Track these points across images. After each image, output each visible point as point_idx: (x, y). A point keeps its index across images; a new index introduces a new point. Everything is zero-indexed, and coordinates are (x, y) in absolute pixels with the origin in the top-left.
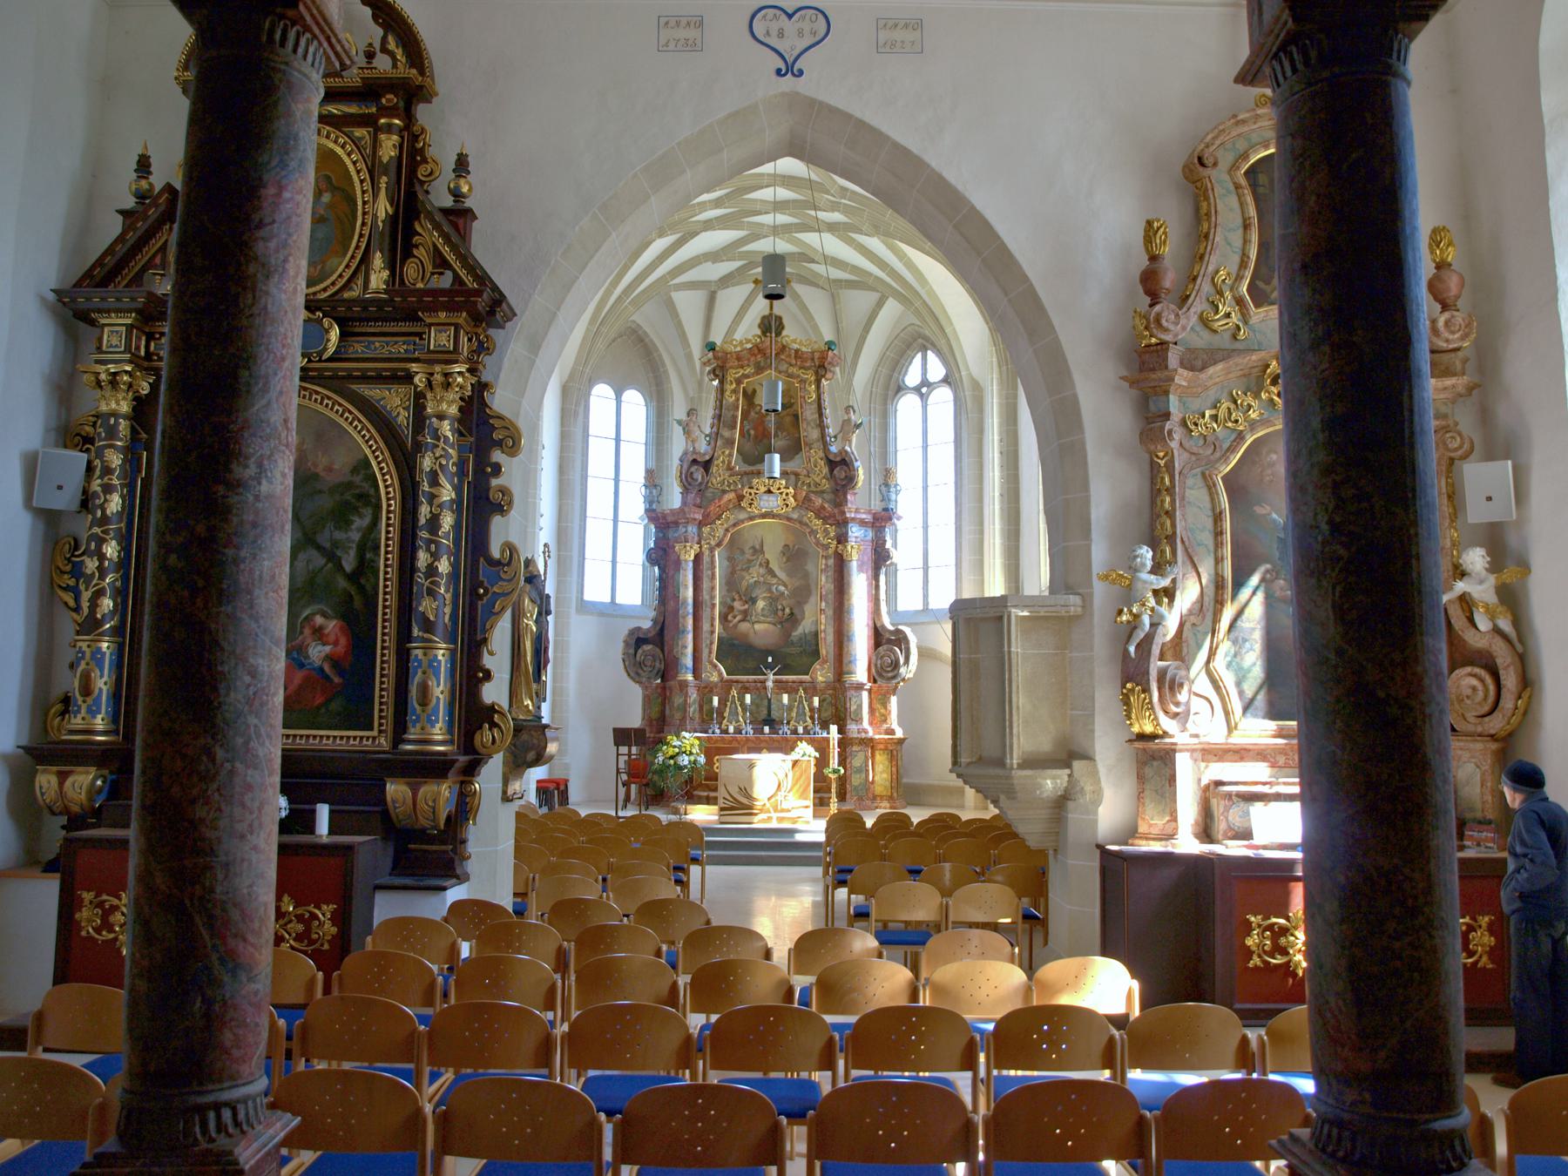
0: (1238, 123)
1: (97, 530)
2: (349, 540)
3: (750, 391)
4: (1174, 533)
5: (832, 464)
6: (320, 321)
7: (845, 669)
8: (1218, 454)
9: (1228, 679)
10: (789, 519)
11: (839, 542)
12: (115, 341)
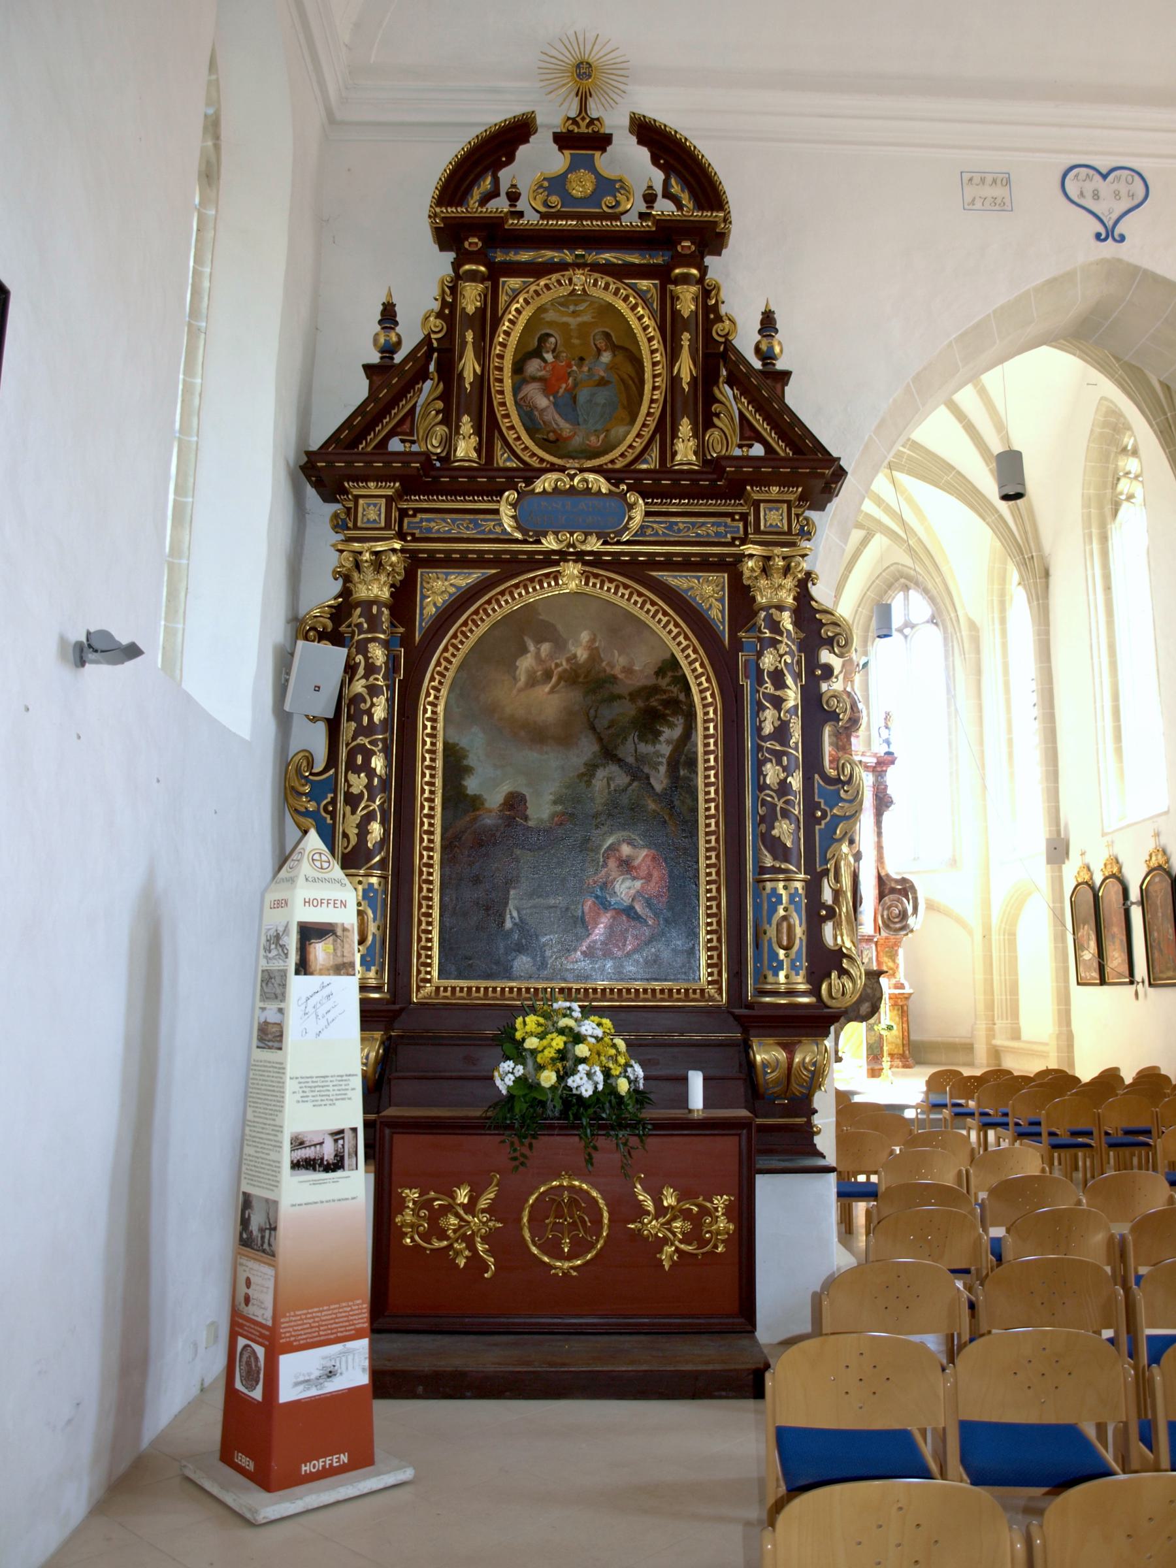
1: (362, 740)
2: (658, 754)
6: (623, 495)
12: (372, 516)
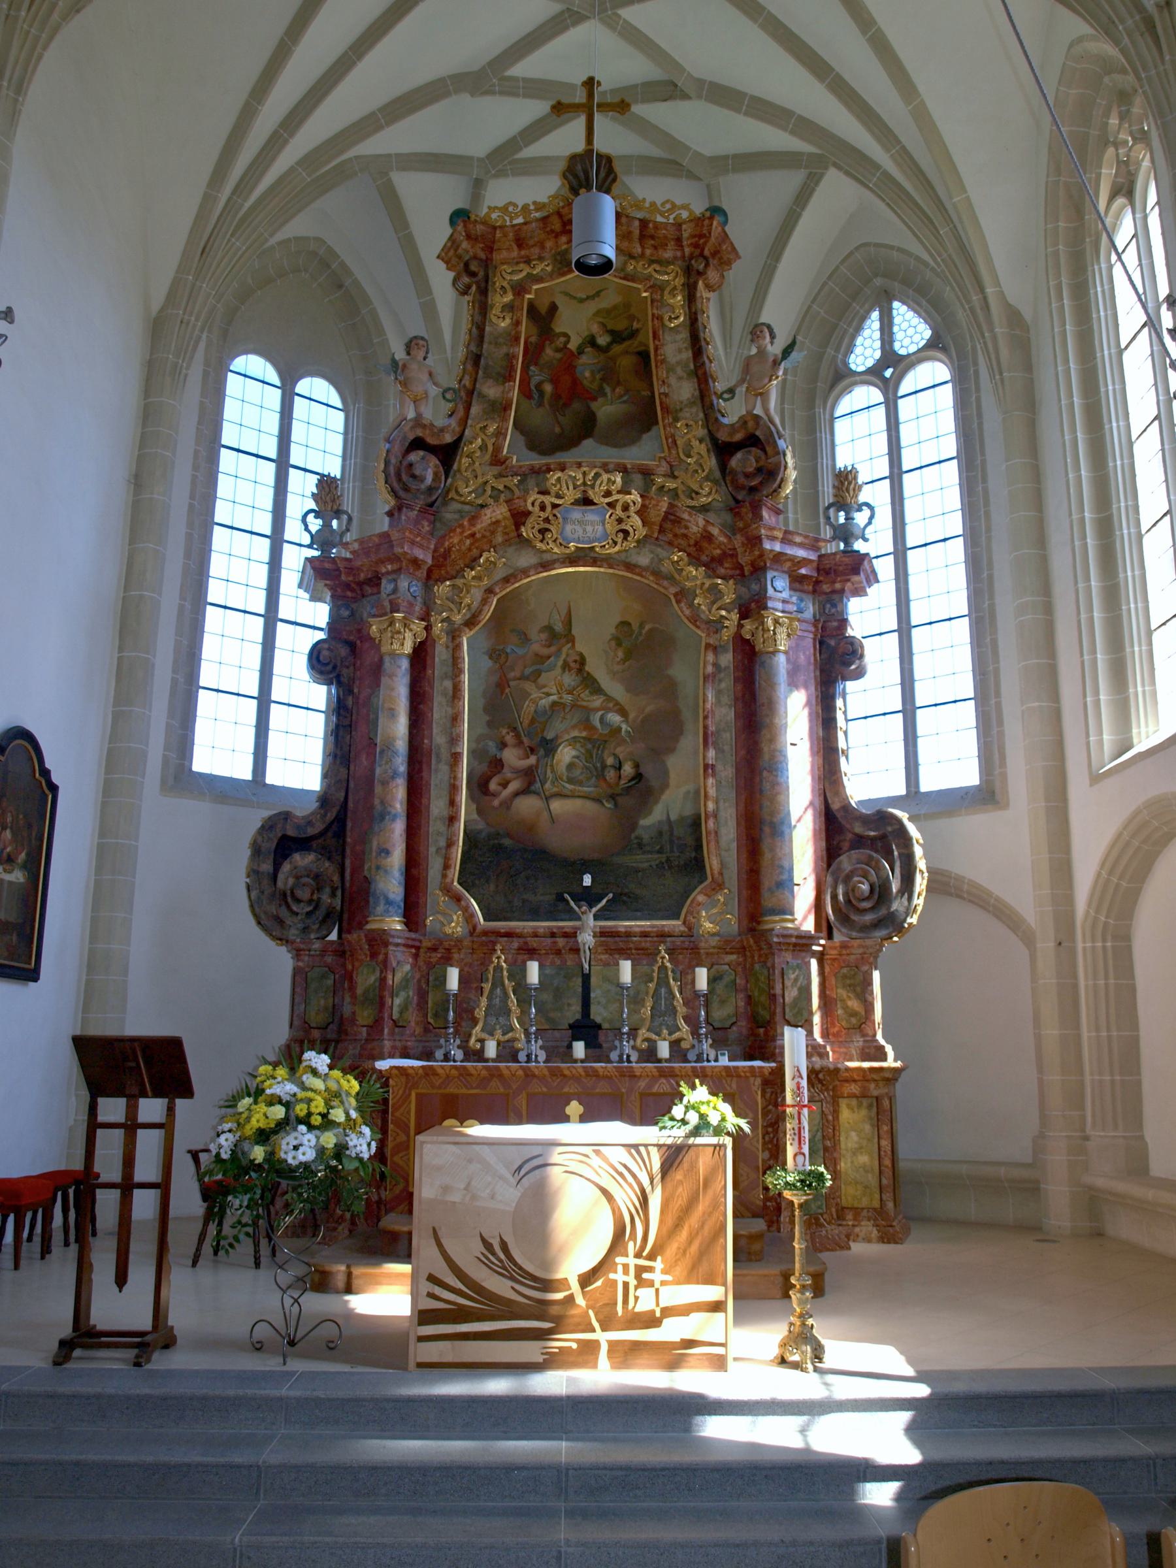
3: (543, 309)
5: (723, 450)
7: (768, 901)
10: (630, 567)
11: (744, 614)
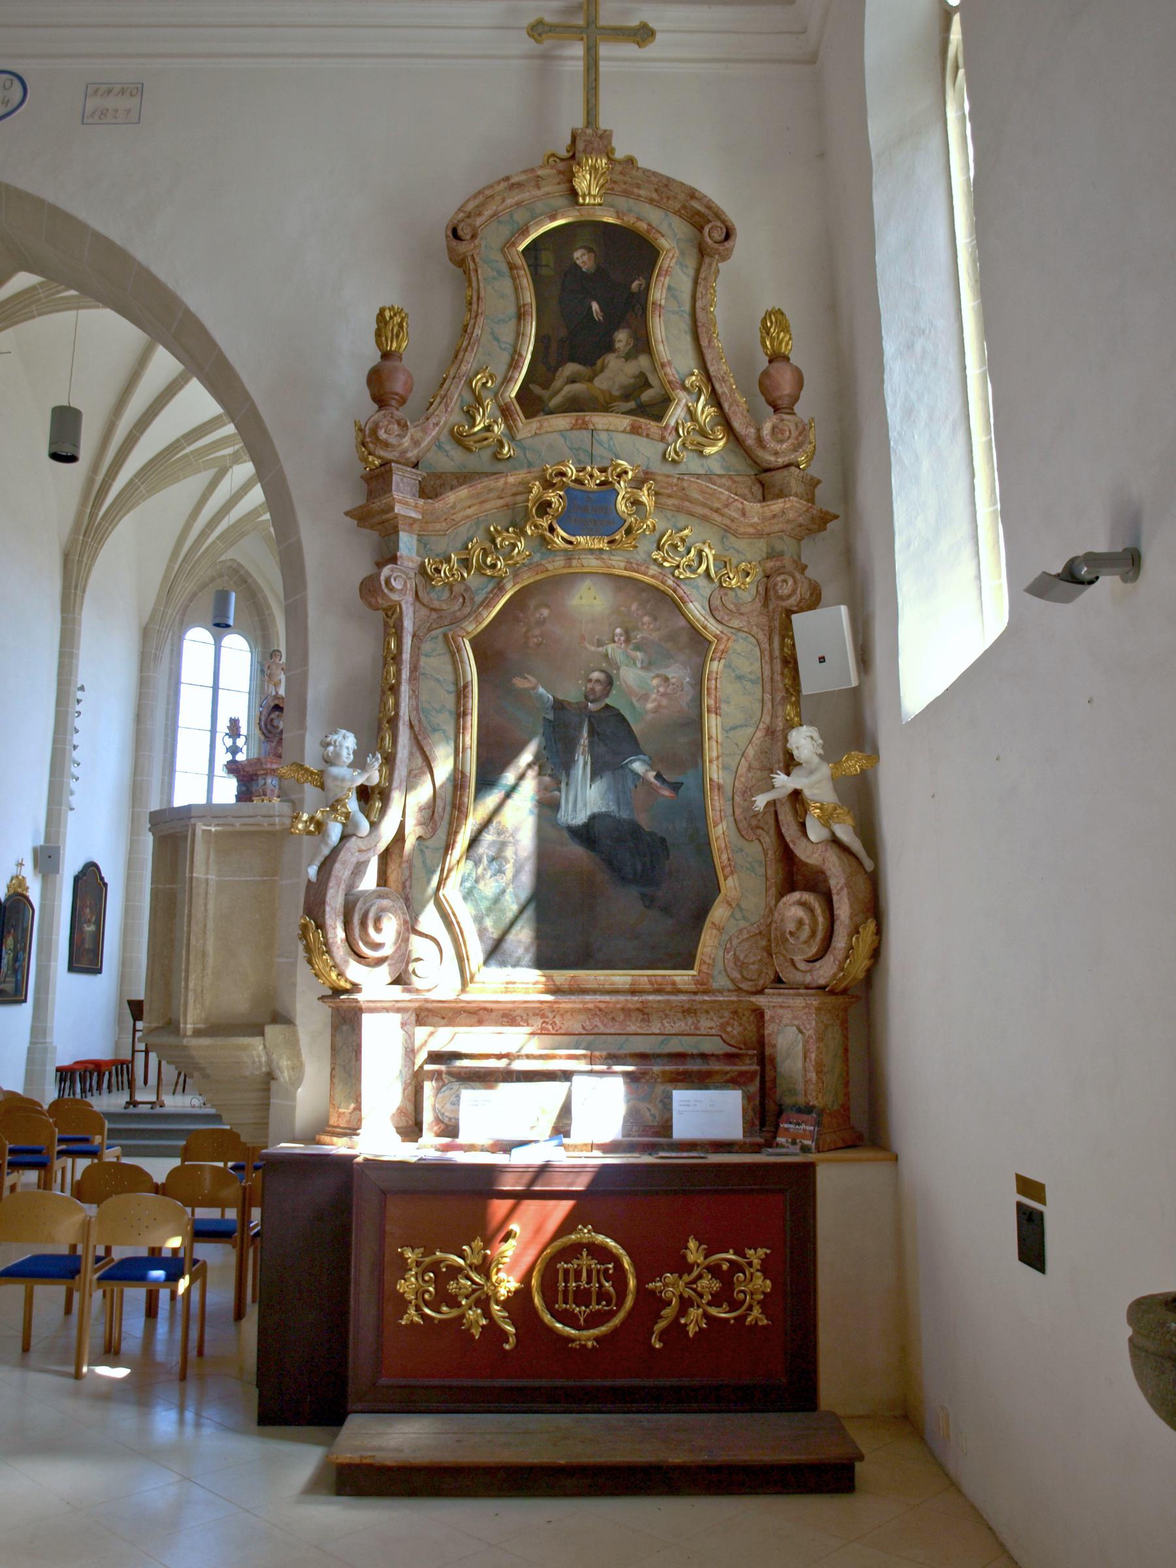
0: (512, 187)
4: (397, 714)
8: (467, 610)
9: (464, 914)
